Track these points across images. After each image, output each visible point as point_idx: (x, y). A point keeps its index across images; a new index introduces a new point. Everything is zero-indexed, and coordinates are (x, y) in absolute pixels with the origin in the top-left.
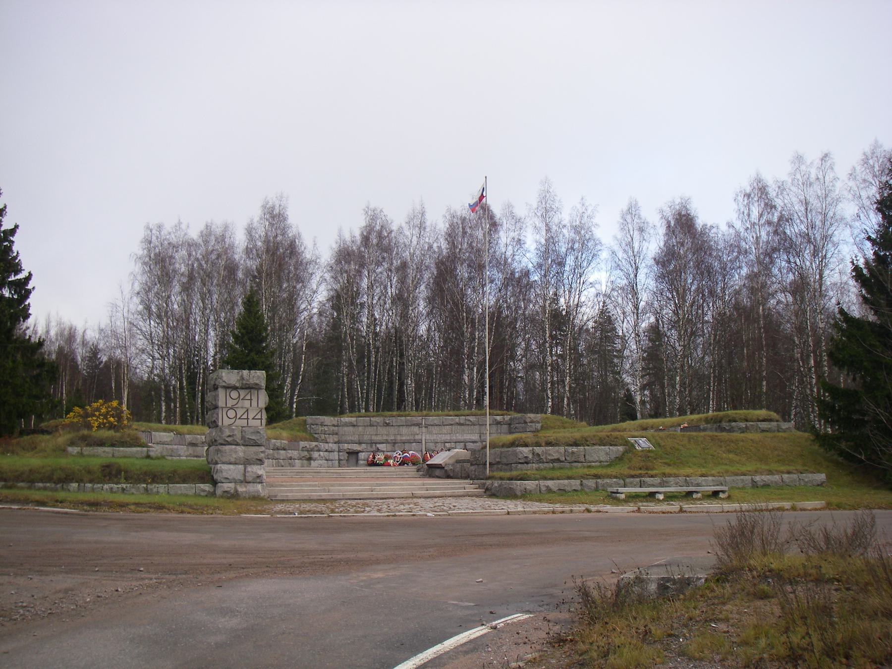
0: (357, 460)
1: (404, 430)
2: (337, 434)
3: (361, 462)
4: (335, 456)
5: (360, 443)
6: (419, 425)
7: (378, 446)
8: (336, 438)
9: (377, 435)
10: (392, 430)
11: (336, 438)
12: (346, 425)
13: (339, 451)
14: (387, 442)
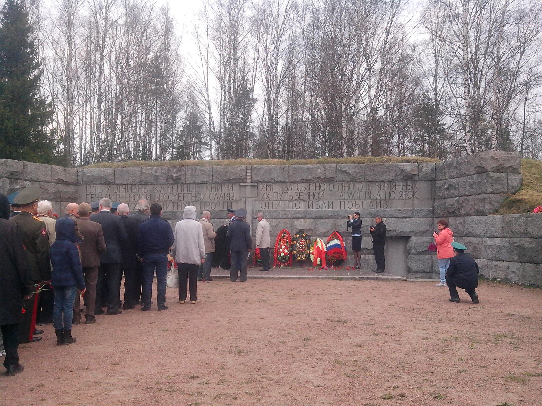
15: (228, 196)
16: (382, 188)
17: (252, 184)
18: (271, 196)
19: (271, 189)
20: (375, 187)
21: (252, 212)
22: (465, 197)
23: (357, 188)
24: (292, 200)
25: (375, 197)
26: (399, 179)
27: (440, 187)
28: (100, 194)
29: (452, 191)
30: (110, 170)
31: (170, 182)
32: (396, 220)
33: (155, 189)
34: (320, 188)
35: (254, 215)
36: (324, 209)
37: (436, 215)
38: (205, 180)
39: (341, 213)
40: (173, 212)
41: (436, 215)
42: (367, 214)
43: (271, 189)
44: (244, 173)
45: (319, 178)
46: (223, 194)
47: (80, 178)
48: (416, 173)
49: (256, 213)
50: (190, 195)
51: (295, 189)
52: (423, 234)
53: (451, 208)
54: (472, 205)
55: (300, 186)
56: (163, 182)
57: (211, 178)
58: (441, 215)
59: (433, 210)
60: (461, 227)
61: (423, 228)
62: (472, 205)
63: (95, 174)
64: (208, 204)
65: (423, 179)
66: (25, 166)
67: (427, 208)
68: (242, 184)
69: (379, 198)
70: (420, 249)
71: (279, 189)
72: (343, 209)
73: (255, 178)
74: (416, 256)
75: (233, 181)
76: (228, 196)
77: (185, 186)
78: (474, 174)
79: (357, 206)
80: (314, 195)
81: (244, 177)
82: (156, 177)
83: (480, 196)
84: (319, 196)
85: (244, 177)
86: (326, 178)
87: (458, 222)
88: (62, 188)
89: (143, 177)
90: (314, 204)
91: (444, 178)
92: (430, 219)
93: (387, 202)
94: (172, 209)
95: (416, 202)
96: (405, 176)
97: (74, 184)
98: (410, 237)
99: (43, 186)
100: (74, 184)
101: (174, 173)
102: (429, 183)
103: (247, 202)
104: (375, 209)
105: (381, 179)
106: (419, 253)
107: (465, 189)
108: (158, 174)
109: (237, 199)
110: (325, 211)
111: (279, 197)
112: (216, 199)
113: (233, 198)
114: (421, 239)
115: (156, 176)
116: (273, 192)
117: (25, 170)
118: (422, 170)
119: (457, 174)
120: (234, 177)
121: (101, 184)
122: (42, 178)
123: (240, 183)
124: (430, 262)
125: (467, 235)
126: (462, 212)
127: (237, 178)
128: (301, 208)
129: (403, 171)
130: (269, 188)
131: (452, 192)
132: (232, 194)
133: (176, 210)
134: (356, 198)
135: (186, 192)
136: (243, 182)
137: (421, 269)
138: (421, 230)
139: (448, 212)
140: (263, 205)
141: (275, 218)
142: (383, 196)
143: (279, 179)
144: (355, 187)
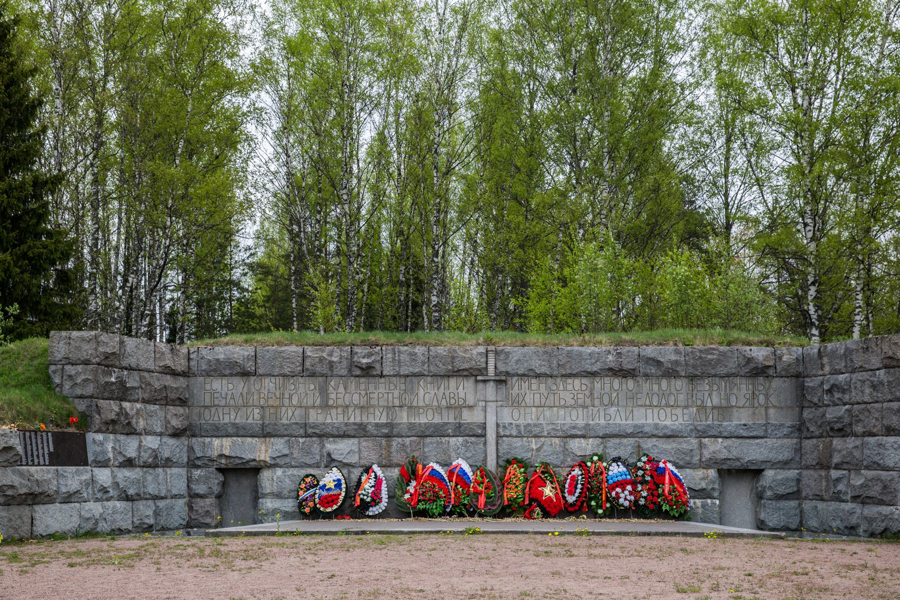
0: (256, 496)
1: (426, 393)
2: (182, 402)
3: (269, 504)
4: (175, 479)
5: (265, 433)
6: (475, 374)
7: (331, 446)
8: (176, 417)
9: (325, 406)
10: (383, 392)
11: (176, 417)
12: (218, 370)
13: (192, 464)
14: (360, 431)
15: (456, 398)
16: (715, 387)
17: (498, 378)
18: (529, 399)
19: (530, 388)
20: (705, 385)
21: (498, 425)
22: (864, 406)
23: (673, 388)
24: (565, 407)
25: (703, 402)
26: (742, 373)
27: (813, 388)
28: (230, 392)
29: (837, 395)
30: (249, 351)
31: (354, 373)
32: (740, 441)
33: (326, 384)
34: (612, 387)
35: (501, 430)
36: (618, 421)
37: (805, 433)
38: (417, 370)
39: (647, 429)
40: (361, 424)
41: (805, 433)
42: (692, 430)
43: (530, 388)
44: (484, 360)
45: (610, 369)
46: (447, 394)
47: (192, 363)
48: (771, 363)
49: (504, 427)
50: (390, 395)
51: (570, 387)
52: (785, 464)
53: (836, 422)
54: (877, 419)
55: (577, 382)
56: (344, 372)
57: (426, 367)
58: (817, 433)
59: (800, 425)
60: (857, 454)
61: (786, 455)
62: (877, 419)
63: (222, 357)
64: (421, 411)
65: (783, 373)
66: (122, 343)
67: (789, 421)
68: (479, 378)
69: (709, 404)
70: (781, 490)
71: (543, 386)
72: (650, 421)
73: (502, 368)
74: (774, 503)
75: (465, 373)
76: (456, 398)
77: (382, 380)
78: (878, 369)
79: (674, 418)
80: (601, 398)
81: (484, 365)
82: (331, 365)
83: (892, 404)
84: (610, 398)
85: (484, 365)
86: (622, 370)
87: (850, 446)
88: (169, 381)
89: (308, 364)
90: (602, 413)
91: (820, 372)
92: (795, 441)
93: (724, 410)
94: (358, 420)
95: (772, 411)
96: (754, 369)
97: (185, 374)
98: (763, 470)
99: (145, 378)
100: (185, 374)
101: (364, 358)
102: (794, 380)
103: (489, 409)
104: (704, 423)
105: (713, 372)
106: (779, 497)
107: (862, 392)
108: (334, 359)
109: (471, 404)
110: (620, 425)
111: (543, 401)
112: (435, 403)
113: (465, 401)
114: (782, 475)
115: (331, 362)
116: (532, 392)
117: (122, 350)
118: (780, 358)
119: (845, 366)
120: (466, 366)
121: (231, 375)
122: (144, 365)
123: (476, 376)
124: (798, 511)
125: (867, 468)
126: (859, 429)
127: (471, 368)
128: (578, 419)
129: (749, 360)
130: (525, 385)
131: (836, 396)
132: (462, 395)
133: (365, 420)
134: (672, 404)
135: (382, 390)
136: (482, 375)
137: (782, 524)
138: (780, 458)
139: (832, 429)
140: (516, 415)
141: (535, 436)
142: (716, 401)
143: (543, 370)
144: (669, 385)
